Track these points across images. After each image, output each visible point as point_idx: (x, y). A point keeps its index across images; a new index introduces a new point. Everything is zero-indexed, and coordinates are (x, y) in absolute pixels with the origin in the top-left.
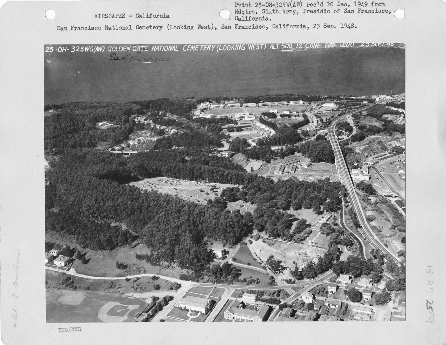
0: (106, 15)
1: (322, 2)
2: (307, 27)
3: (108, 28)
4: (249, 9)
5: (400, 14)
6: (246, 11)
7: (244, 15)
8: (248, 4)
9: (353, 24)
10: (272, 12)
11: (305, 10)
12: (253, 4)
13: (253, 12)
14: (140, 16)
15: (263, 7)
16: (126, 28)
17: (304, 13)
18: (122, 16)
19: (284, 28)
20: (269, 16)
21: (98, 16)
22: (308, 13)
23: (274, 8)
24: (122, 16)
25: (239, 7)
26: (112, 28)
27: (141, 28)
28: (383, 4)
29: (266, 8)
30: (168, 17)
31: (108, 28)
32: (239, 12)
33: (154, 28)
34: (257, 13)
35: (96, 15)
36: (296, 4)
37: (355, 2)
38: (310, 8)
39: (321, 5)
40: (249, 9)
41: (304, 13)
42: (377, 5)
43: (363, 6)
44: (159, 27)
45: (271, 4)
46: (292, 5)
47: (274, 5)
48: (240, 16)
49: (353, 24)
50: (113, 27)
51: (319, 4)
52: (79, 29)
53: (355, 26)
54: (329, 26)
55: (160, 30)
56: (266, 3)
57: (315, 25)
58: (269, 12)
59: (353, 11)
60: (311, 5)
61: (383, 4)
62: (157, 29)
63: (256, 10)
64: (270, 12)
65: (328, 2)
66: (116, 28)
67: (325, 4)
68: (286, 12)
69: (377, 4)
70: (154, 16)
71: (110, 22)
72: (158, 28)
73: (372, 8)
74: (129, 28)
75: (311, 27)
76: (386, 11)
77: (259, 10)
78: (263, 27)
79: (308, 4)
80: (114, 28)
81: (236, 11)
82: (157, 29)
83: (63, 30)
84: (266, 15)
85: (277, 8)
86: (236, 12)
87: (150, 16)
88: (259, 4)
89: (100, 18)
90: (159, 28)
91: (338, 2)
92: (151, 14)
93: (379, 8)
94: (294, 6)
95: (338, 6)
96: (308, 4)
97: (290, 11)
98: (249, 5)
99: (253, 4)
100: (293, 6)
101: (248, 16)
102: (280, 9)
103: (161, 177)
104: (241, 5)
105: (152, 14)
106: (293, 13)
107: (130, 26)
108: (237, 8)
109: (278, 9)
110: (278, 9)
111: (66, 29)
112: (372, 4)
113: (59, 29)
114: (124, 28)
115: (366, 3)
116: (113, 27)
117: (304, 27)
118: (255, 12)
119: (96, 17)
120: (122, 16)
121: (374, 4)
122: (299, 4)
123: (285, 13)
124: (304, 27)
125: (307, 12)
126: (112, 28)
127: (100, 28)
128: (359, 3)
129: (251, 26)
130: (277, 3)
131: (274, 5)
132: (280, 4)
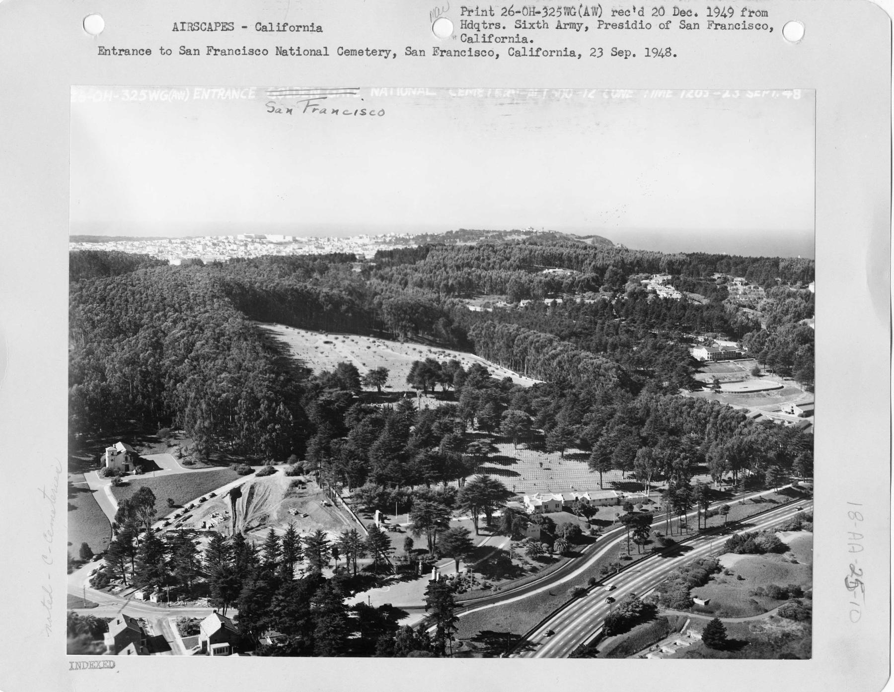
0: (196, 24)
1: (643, 8)
2: (577, 54)
3: (281, 52)
4: (489, 19)
5: (794, 31)
6: (484, 23)
7: (479, 31)
8: (488, 9)
9: (669, 48)
10: (535, 26)
11: (601, 23)
12: (498, 11)
13: (498, 26)
14: (264, 29)
15: (518, 16)
16: (318, 53)
17: (599, 28)
18: (227, 26)
19: (532, 55)
20: (528, 34)
21: (180, 27)
22: (606, 28)
23: (538, 18)
24: (227, 26)
25: (469, 15)
26: (289, 52)
27: (348, 52)
28: (765, 14)
29: (522, 18)
30: (319, 29)
31: (281, 52)
32: (470, 26)
33: (374, 52)
34: (504, 28)
35: (175, 24)
36: (590, 11)
37: (709, 8)
38: (618, 19)
39: (641, 13)
40: (489, 19)
41: (599, 28)
42: (752, 14)
43: (725, 16)
44: (383, 51)
45: (532, 10)
46: (582, 13)
47: (539, 13)
48: (471, 33)
49: (669, 48)
50: (291, 50)
51: (637, 10)
52: (224, 53)
53: (673, 53)
54: (620, 53)
55: (386, 57)
56: (524, 8)
57: (593, 50)
58: (528, 26)
59: (649, 26)
60: (621, 13)
61: (765, 14)
62: (380, 55)
63: (503, 21)
64: (532, 25)
65: (505, 8)
66: (297, 53)
67: (648, 12)
68: (563, 26)
69: (753, 12)
70: (292, 29)
71: (288, 40)
72: (382, 53)
73: (740, 20)
74: (323, 52)
75: (586, 54)
76: (765, 27)
77: (509, 22)
78: (491, 53)
79: (614, 12)
80: (293, 52)
81: (464, 23)
82: (380, 55)
83: (190, 54)
84: (522, 33)
85: (544, 18)
86: (464, 26)
87: (283, 28)
88: (556, 10)
89: (183, 30)
90: (384, 54)
91: (674, 8)
92: (285, 25)
93: (755, 20)
94: (586, 14)
95: (674, 15)
96: (614, 12)
97: (572, 25)
98: (488, 13)
99: (498, 11)
100: (585, 15)
101: (488, 32)
102: (552, 21)
103: (637, 627)
104: (472, 11)
105: (287, 24)
106: (578, 28)
107: (326, 48)
108: (465, 17)
109: (547, 19)
110: (548, 19)
111: (197, 52)
112: (743, 11)
113: (183, 52)
114: (313, 53)
115: (731, 11)
116: (291, 50)
117: (573, 54)
118: (502, 26)
119: (175, 29)
120: (226, 27)
121: (747, 13)
122: (597, 10)
123: (561, 28)
124: (573, 54)
125: (604, 26)
126: (289, 52)
127: (266, 52)
128: (717, 11)
129: (465, 52)
130: (545, 8)
131: (539, 13)
132: (552, 10)
